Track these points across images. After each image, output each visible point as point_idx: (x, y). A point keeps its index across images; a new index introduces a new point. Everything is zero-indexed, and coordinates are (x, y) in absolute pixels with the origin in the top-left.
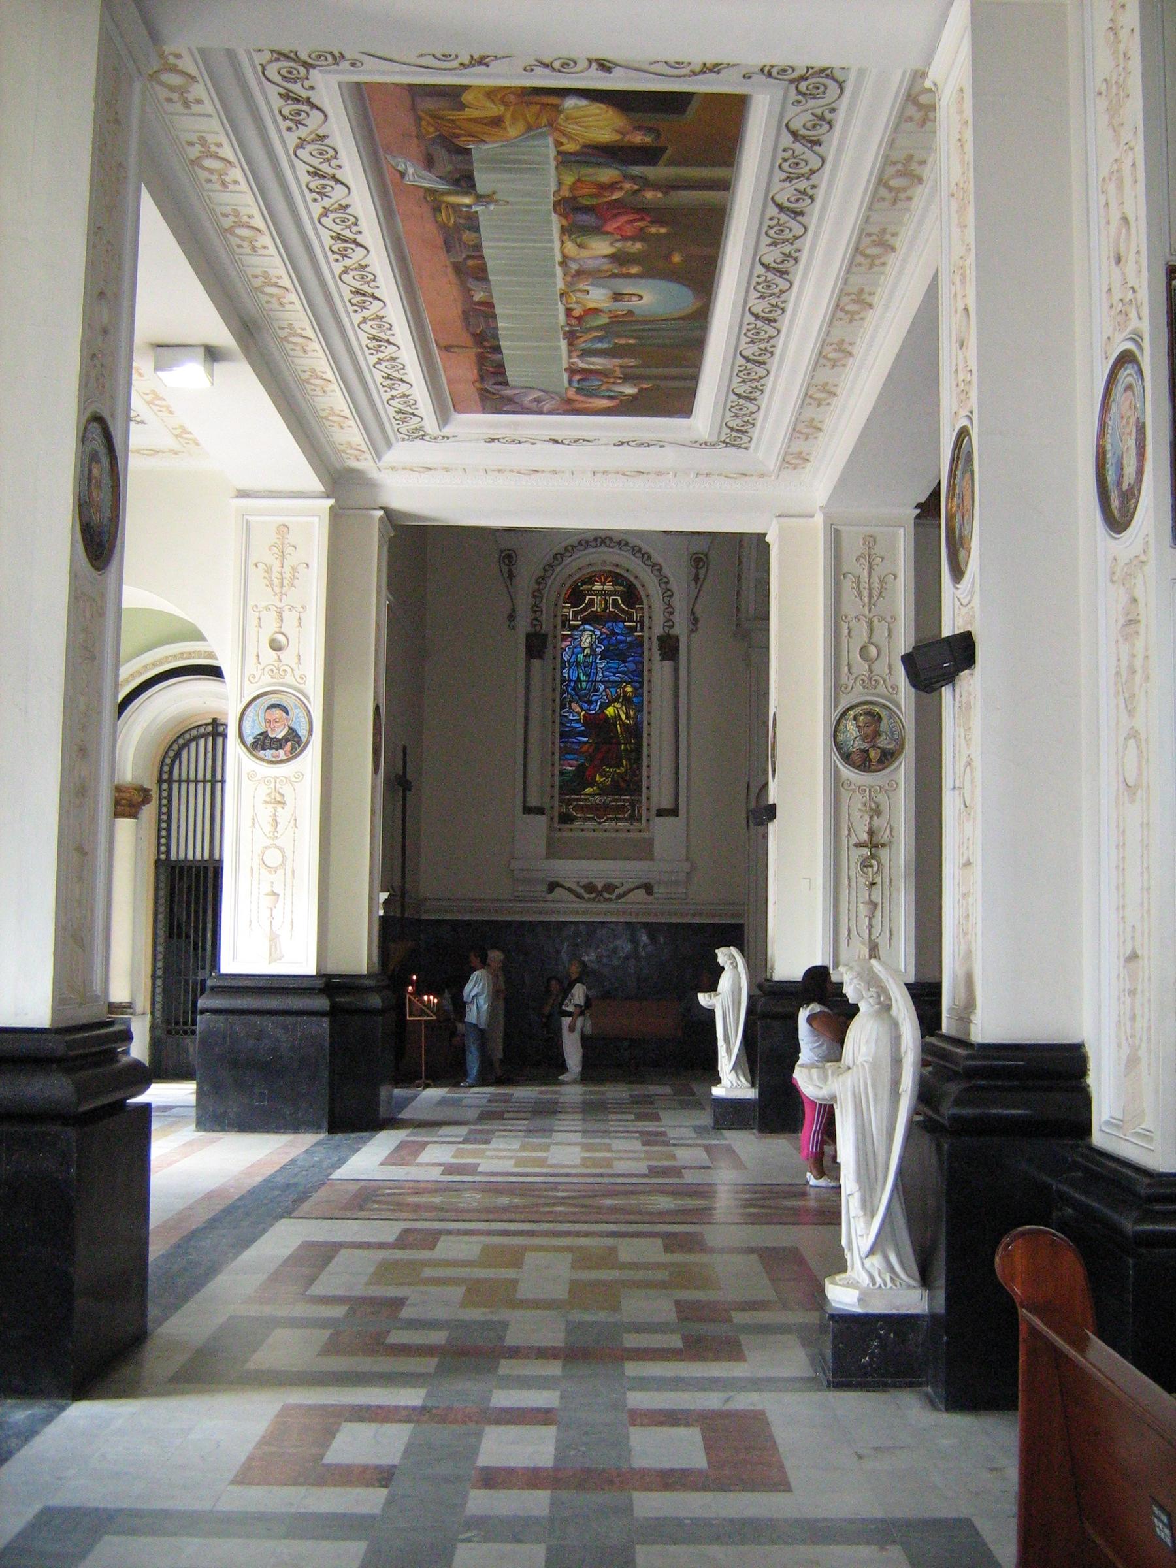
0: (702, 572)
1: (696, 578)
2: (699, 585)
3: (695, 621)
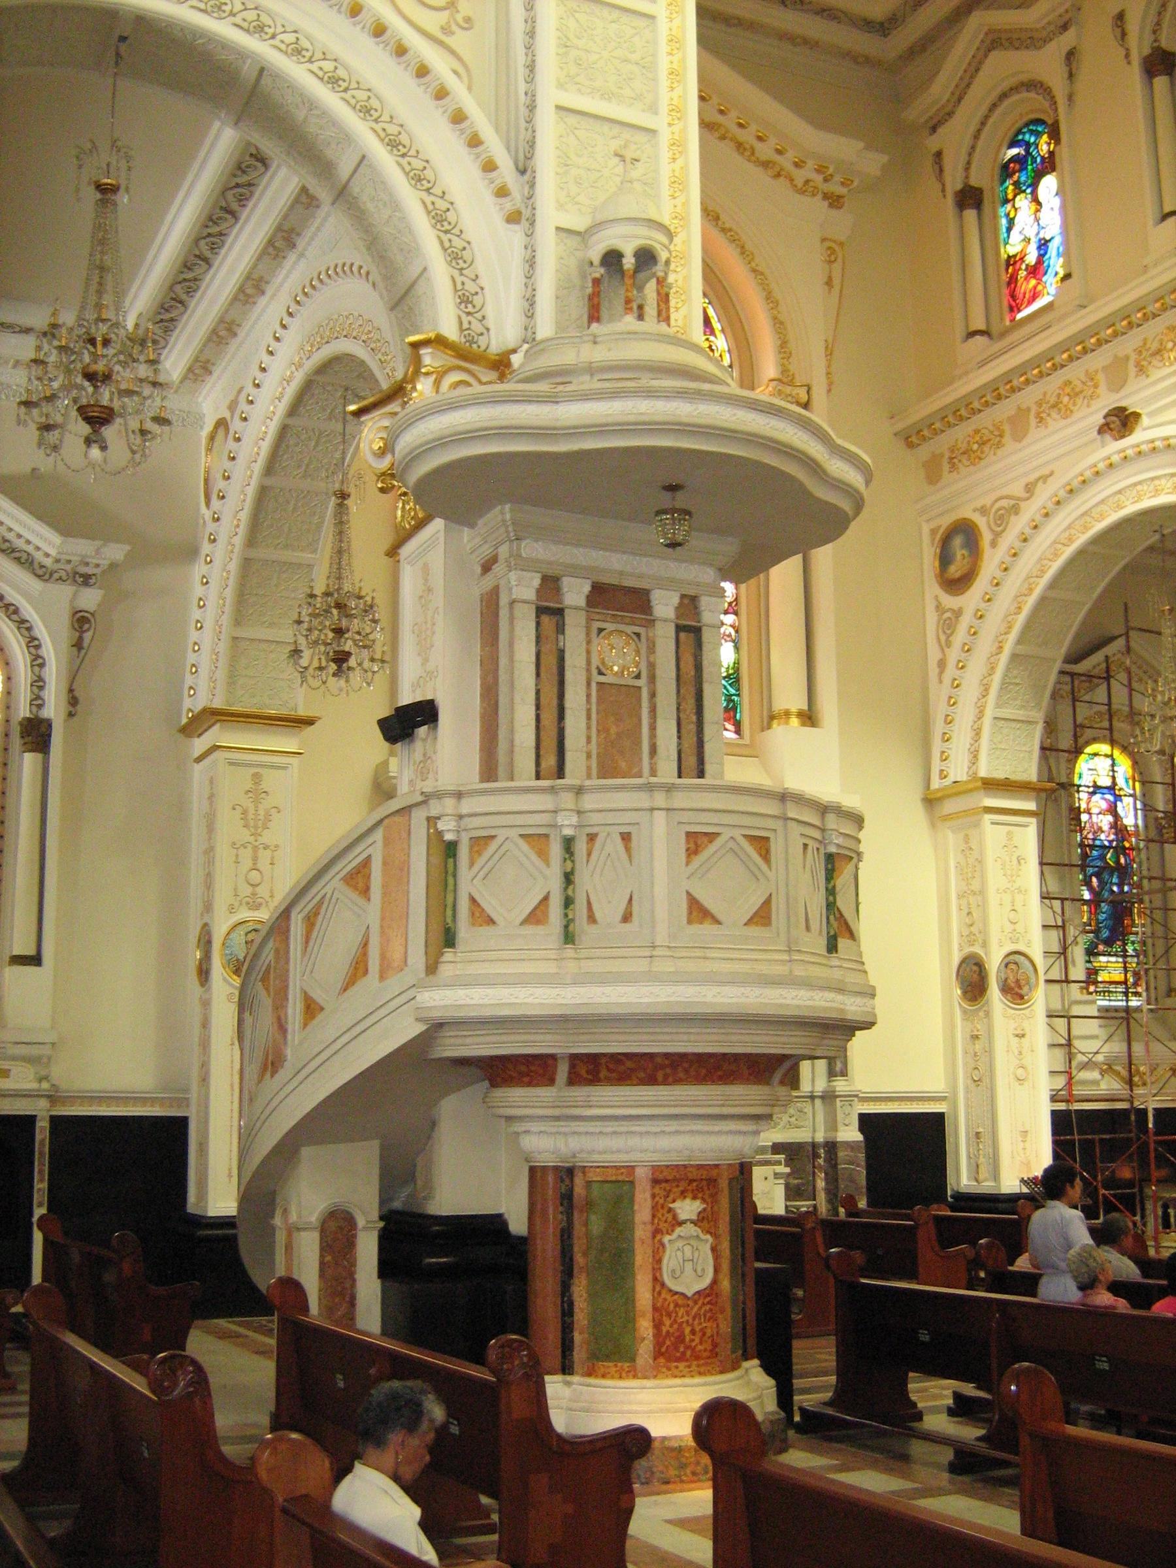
0: (87, 636)
1: (78, 645)
2: (83, 652)
3: (73, 701)
